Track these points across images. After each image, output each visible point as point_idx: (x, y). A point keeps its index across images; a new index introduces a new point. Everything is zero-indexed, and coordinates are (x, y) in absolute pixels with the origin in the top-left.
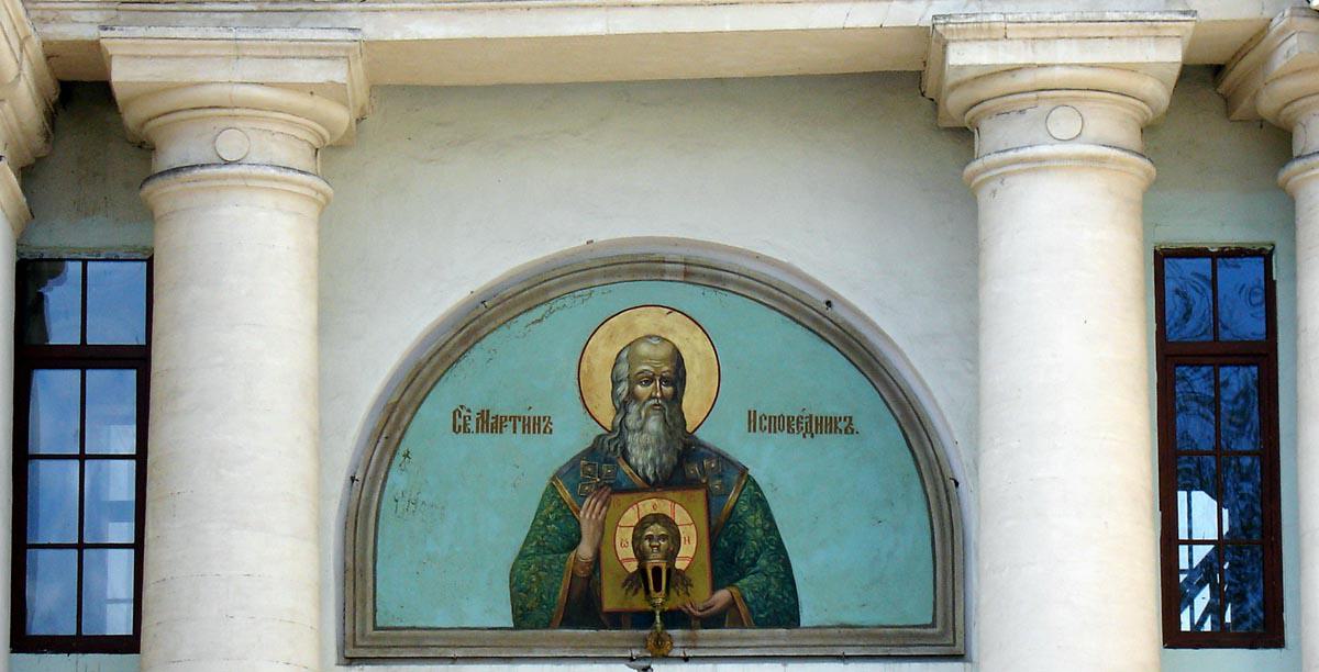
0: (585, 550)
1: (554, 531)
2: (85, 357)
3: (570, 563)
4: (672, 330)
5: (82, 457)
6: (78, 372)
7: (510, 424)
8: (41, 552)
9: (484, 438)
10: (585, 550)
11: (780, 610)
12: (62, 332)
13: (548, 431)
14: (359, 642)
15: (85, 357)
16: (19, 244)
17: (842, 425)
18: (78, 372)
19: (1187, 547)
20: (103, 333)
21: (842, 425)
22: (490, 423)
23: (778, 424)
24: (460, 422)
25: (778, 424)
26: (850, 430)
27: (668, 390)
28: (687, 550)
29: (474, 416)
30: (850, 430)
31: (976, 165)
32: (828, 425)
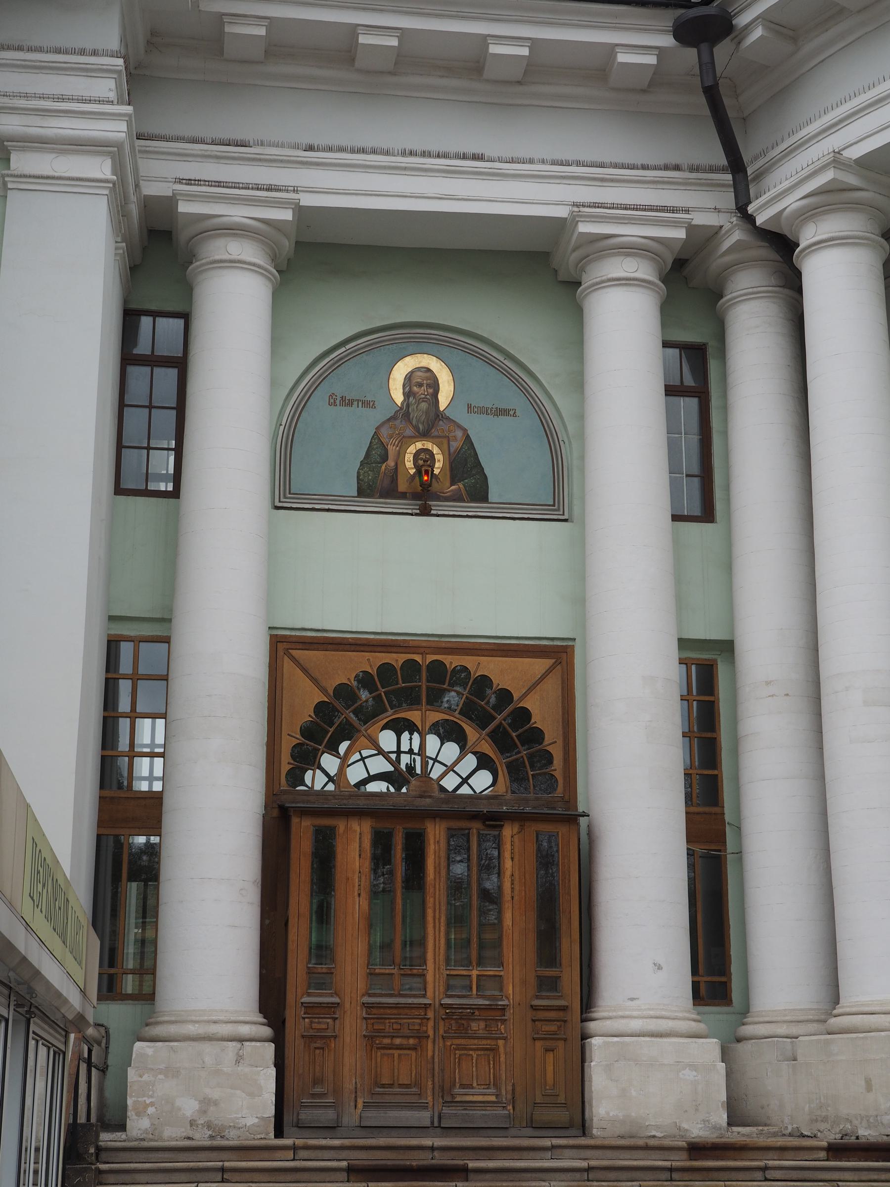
0: (391, 463)
1: (376, 454)
2: (153, 361)
3: (383, 467)
4: (420, 362)
5: (150, 407)
6: (174, 405)
7: (356, 403)
8: (128, 450)
9: (343, 408)
10: (391, 463)
11: (479, 493)
12: (143, 347)
13: (374, 407)
14: (282, 500)
15: (153, 361)
16: (125, 301)
17: (512, 413)
18: (174, 405)
19: (150, 319)
20: (163, 350)
21: (512, 413)
22: (347, 402)
23: (483, 411)
24: (332, 401)
25: (483, 411)
26: (514, 415)
27: (431, 391)
28: (438, 465)
29: (339, 399)
30: (514, 415)
31: (724, 299)
32: (504, 412)
